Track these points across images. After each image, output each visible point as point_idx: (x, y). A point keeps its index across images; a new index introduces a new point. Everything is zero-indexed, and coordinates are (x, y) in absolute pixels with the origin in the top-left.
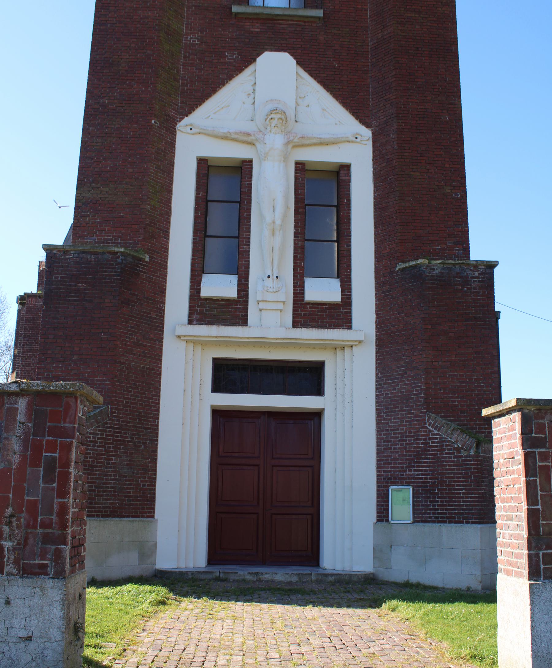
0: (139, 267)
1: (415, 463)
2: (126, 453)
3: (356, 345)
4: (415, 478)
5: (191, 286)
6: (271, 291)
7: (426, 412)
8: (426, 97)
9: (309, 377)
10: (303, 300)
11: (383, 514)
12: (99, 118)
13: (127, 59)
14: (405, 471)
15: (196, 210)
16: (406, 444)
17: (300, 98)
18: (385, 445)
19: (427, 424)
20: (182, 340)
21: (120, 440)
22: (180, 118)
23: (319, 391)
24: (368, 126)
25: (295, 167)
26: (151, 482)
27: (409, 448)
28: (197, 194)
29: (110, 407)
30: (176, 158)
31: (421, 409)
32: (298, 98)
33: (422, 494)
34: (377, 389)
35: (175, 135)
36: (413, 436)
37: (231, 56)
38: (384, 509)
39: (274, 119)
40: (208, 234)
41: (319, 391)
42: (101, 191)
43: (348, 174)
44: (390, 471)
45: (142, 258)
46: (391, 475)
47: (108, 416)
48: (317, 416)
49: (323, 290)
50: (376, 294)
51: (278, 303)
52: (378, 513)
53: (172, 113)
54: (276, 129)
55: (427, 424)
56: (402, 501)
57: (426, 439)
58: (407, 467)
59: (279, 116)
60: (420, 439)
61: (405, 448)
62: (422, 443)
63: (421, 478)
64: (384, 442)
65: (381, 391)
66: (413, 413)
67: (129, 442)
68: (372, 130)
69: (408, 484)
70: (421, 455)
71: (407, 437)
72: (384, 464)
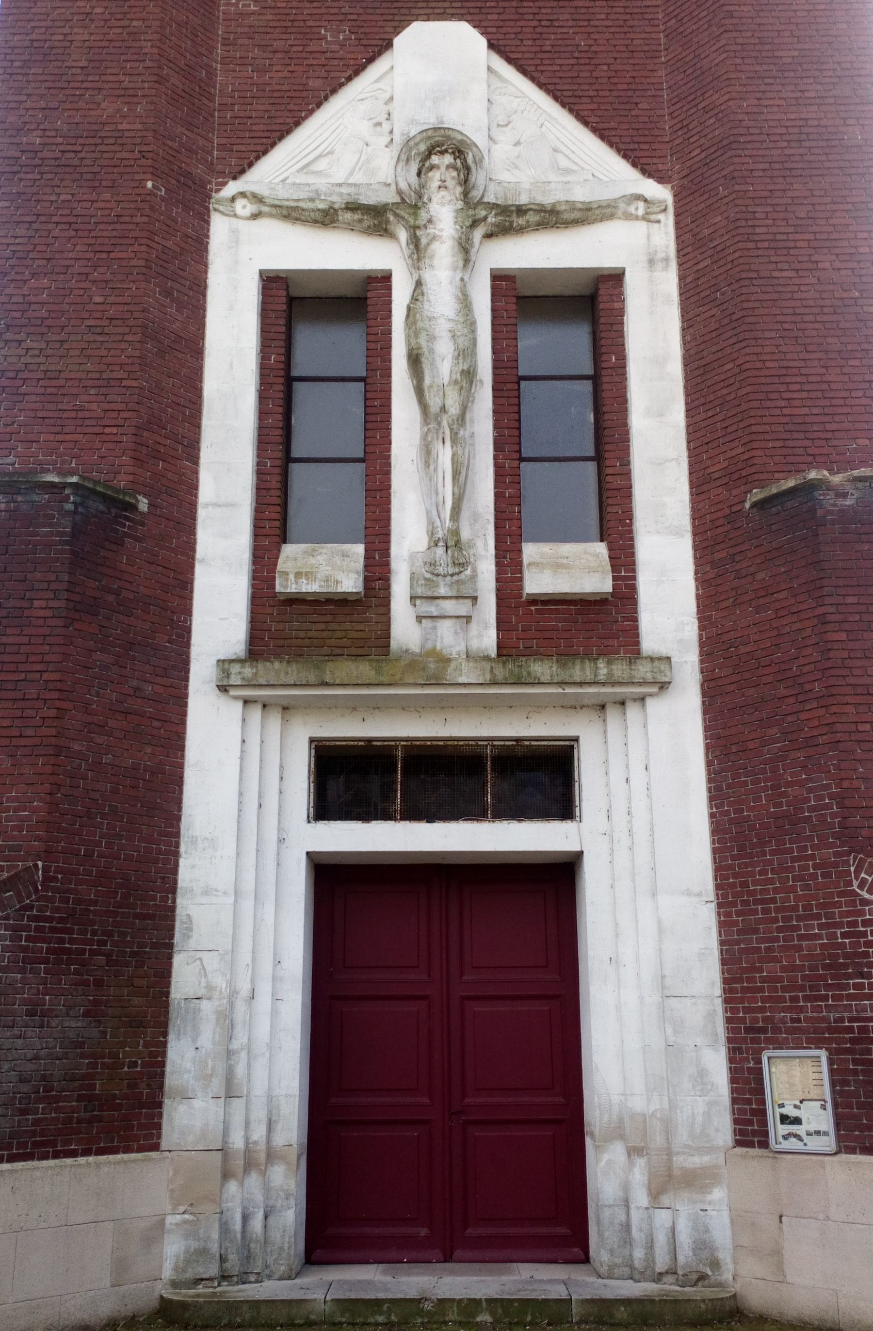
0: (124, 526)
1: (828, 987)
2: (86, 983)
3: (651, 695)
4: (830, 1030)
5: (254, 571)
6: (334, 23)
7: (848, 854)
8: (803, 91)
9: (543, 779)
10: (520, 596)
11: (752, 1123)
12: (21, 180)
13: (85, 41)
14: (801, 1009)
15: (263, 397)
16: (801, 937)
17: (498, 125)
18: (743, 941)
19: (855, 883)
20: (236, 698)
21: (68, 951)
22: (217, 184)
23: (563, 806)
24: (661, 180)
25: (493, 288)
26: (152, 1055)
27: (809, 948)
28: (263, 358)
29: (40, 864)
30: (210, 275)
31: (833, 845)
32: (494, 127)
33: (855, 1072)
34: (711, 799)
35: (208, 223)
36: (818, 917)
37: (333, 37)
38: (753, 1112)
39: (437, 167)
40: (295, 454)
41: (563, 806)
42: (28, 349)
43: (619, 296)
44: (762, 1010)
45: (129, 503)
46: (765, 1019)
47: (36, 890)
48: (558, 877)
49: (564, 568)
50: (696, 573)
51: (461, 601)
52: (736, 1121)
53: (199, 170)
54: (443, 193)
55: (855, 883)
56: (799, 1081)
57: (854, 924)
58: (807, 998)
59: (448, 159)
60: (840, 925)
61: (799, 948)
62: (844, 935)
63: (850, 1030)
64: (740, 932)
65: (722, 805)
66: (813, 857)
67: (93, 953)
68: (673, 187)
69: (817, 1043)
70: (845, 966)
71: (799, 918)
72: (745, 990)
